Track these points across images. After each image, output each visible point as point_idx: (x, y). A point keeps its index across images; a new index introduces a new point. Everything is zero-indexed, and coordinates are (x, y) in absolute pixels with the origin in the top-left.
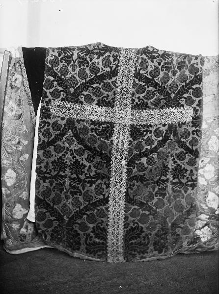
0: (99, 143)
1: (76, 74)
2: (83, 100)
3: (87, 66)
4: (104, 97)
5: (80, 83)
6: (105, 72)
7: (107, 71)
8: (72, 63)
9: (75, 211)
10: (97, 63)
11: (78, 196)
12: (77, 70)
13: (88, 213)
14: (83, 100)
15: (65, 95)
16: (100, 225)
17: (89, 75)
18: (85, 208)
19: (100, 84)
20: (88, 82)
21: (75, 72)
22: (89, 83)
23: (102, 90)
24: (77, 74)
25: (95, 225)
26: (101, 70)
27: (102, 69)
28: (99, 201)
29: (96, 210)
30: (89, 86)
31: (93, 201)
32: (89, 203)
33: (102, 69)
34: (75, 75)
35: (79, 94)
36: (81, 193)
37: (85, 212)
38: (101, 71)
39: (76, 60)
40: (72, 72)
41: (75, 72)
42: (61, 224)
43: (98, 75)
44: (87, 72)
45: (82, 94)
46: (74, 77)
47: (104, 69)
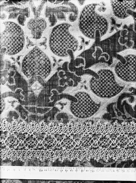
0: (112, 43)
1: (43, 44)
2: (67, 110)
3: (72, 19)
4: (124, 95)
5: (56, 67)
6: (121, 28)
7: (125, 27)
8: (32, 16)
9: (62, 63)
10: (97, 7)
11: (67, 21)
12: (47, 33)
13: (95, 68)
14: (67, 110)
15: (17, 104)
16: (127, 99)
17: (79, 41)
18: (87, 53)
19: (110, 63)
20: (78, 61)
21: (41, 40)
22: (82, 61)
23: (118, 80)
24: (47, 43)
25: (114, 99)
26: (110, 26)
27: (113, 22)
28: (124, 32)
29: (115, 61)
30: (81, 72)
31: (108, 34)
32: (97, 42)
33: (113, 22)
34: (42, 48)
35: (56, 98)
36: (76, 12)
37: (88, 65)
38: (112, 29)
39: (40, 8)
40: (33, 41)
41: (41, 40)
42: (23, 106)
43: (103, 38)
44: (72, 33)
45: (63, 96)
46: (39, 52)
47: (119, 20)
